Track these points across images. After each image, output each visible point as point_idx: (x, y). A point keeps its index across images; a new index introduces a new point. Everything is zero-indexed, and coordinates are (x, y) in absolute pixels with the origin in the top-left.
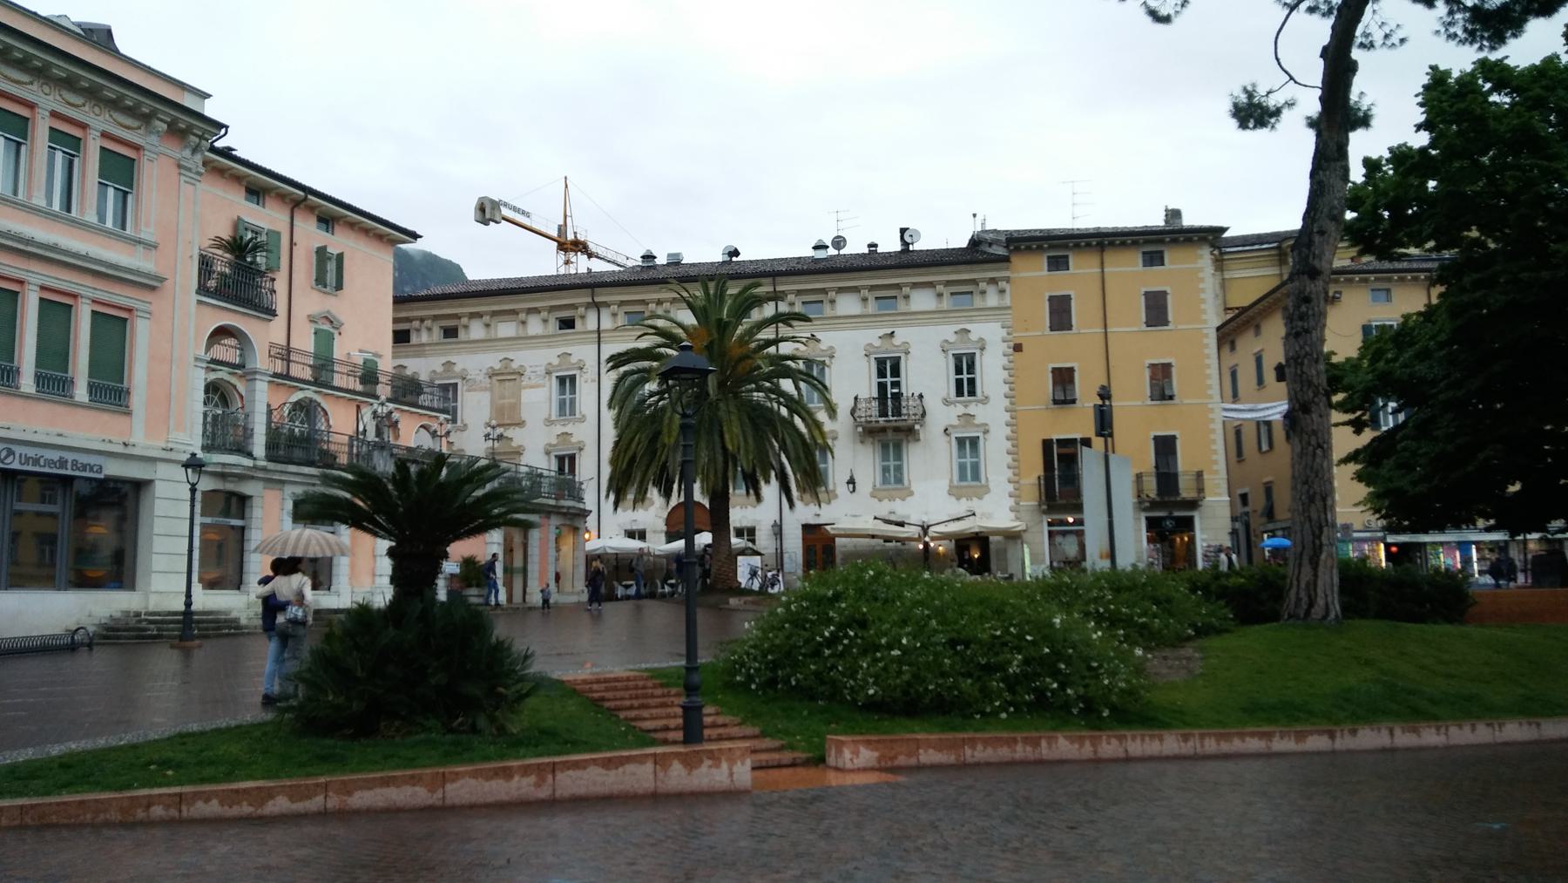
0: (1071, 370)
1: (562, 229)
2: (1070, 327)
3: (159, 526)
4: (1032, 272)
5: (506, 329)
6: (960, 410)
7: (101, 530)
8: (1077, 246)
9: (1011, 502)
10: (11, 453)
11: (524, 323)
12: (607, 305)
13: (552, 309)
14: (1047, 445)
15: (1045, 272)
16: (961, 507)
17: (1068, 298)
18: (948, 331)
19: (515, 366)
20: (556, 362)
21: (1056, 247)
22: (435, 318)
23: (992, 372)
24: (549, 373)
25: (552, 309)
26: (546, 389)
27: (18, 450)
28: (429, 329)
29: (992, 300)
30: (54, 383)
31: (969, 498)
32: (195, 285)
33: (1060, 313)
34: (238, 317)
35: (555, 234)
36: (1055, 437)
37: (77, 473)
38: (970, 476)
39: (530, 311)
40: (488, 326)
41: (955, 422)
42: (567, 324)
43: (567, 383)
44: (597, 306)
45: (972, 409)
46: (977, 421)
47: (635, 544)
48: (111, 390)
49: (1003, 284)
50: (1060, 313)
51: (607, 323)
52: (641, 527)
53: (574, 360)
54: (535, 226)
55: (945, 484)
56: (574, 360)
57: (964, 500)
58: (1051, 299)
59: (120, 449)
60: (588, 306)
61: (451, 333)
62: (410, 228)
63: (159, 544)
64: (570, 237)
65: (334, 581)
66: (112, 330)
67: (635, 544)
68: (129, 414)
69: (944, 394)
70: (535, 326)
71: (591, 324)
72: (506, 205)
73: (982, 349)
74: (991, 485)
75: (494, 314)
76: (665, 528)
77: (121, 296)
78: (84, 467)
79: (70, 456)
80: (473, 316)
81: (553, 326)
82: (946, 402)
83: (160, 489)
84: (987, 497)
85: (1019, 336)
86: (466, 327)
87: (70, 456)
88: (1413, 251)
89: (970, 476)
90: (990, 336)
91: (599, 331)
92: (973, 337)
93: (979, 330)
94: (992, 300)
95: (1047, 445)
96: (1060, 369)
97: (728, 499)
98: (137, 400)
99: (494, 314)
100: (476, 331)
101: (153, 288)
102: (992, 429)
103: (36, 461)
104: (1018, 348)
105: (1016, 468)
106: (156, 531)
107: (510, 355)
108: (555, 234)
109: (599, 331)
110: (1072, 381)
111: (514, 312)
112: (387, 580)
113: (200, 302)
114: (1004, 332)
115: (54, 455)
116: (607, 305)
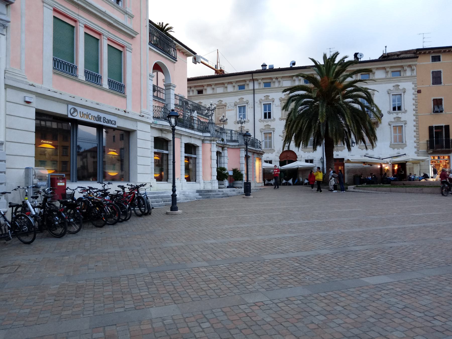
0: (441, 100)
1: (216, 66)
2: (440, 83)
3: (140, 152)
4: (425, 62)
5: (220, 90)
6: (395, 115)
7: (389, 76)
8: (444, 52)
9: (416, 150)
10: (75, 110)
11: (226, 87)
12: (257, 80)
13: (237, 82)
14: (431, 128)
15: (431, 62)
16: (394, 152)
17: (440, 72)
18: (390, 86)
19: (223, 103)
20: (238, 101)
21: (436, 53)
22: (195, 87)
23: (408, 102)
24: (235, 105)
25: (237, 82)
26: (235, 111)
27: (79, 109)
28: (193, 91)
29: (408, 73)
30: (93, 77)
31: (398, 149)
32: (148, 41)
33: (437, 78)
34: (164, 59)
35: (214, 67)
36: (434, 125)
37: (105, 124)
38: (399, 141)
39: (229, 83)
40: (213, 89)
41: (393, 120)
42: (242, 87)
43: (242, 109)
44: (253, 80)
45: (400, 115)
46: (402, 120)
47: (309, 164)
48: (117, 86)
49: (414, 67)
50: (437, 78)
51: (256, 87)
52: (270, 159)
53: (244, 100)
54: (210, 65)
55: (388, 143)
56: (244, 100)
57: (396, 149)
58: (433, 72)
59: (123, 114)
60: (250, 80)
61: (200, 92)
62: (193, 50)
63: (140, 161)
64: (219, 69)
65: (197, 178)
66: (117, 53)
67: (309, 164)
68: (125, 97)
69: (388, 110)
70: (230, 89)
71: (251, 87)
72: (201, 57)
73: (404, 92)
74: (407, 144)
75: (216, 84)
76: (279, 160)
77: (120, 38)
78: (109, 121)
79: (102, 115)
80: (208, 85)
81: (237, 88)
82: (389, 113)
83: (139, 135)
84: (405, 148)
85: (420, 87)
86: (206, 89)
87: (102, 115)
88: (324, 110)
89: (399, 141)
90: (408, 87)
91: (254, 90)
92: (401, 88)
93: (402, 85)
94: (408, 73)
95: (431, 128)
96: (436, 100)
97: (333, 147)
98: (129, 90)
99: (216, 84)
100: (209, 91)
101: (133, 37)
102: (408, 122)
103: (88, 115)
104: (419, 92)
105: (418, 137)
106: (138, 154)
107: (221, 99)
108: (214, 67)
109: (254, 90)
110: (441, 104)
111: (223, 84)
112: (215, 178)
113: (150, 49)
114: (413, 86)
115: (96, 114)
116: (257, 80)
